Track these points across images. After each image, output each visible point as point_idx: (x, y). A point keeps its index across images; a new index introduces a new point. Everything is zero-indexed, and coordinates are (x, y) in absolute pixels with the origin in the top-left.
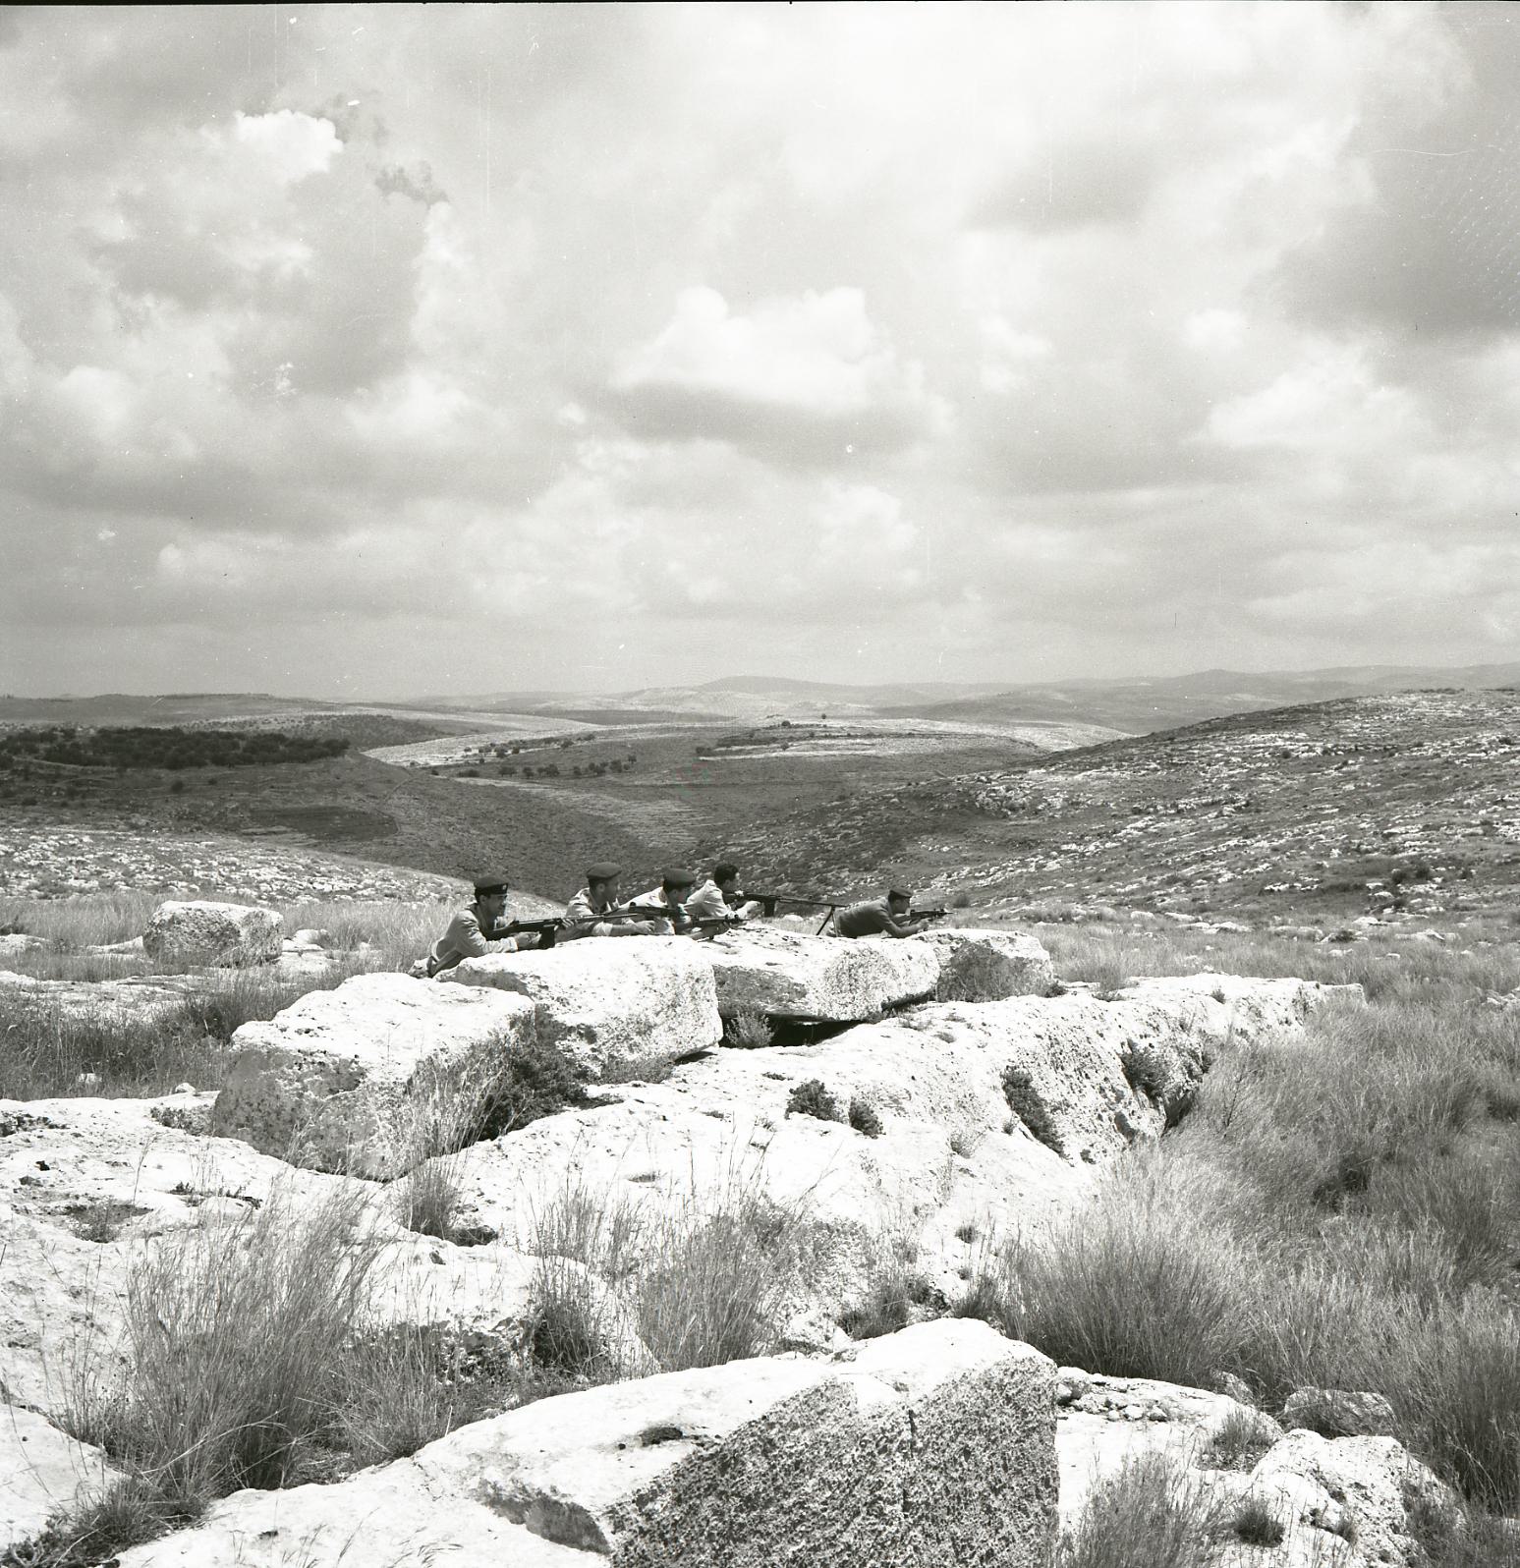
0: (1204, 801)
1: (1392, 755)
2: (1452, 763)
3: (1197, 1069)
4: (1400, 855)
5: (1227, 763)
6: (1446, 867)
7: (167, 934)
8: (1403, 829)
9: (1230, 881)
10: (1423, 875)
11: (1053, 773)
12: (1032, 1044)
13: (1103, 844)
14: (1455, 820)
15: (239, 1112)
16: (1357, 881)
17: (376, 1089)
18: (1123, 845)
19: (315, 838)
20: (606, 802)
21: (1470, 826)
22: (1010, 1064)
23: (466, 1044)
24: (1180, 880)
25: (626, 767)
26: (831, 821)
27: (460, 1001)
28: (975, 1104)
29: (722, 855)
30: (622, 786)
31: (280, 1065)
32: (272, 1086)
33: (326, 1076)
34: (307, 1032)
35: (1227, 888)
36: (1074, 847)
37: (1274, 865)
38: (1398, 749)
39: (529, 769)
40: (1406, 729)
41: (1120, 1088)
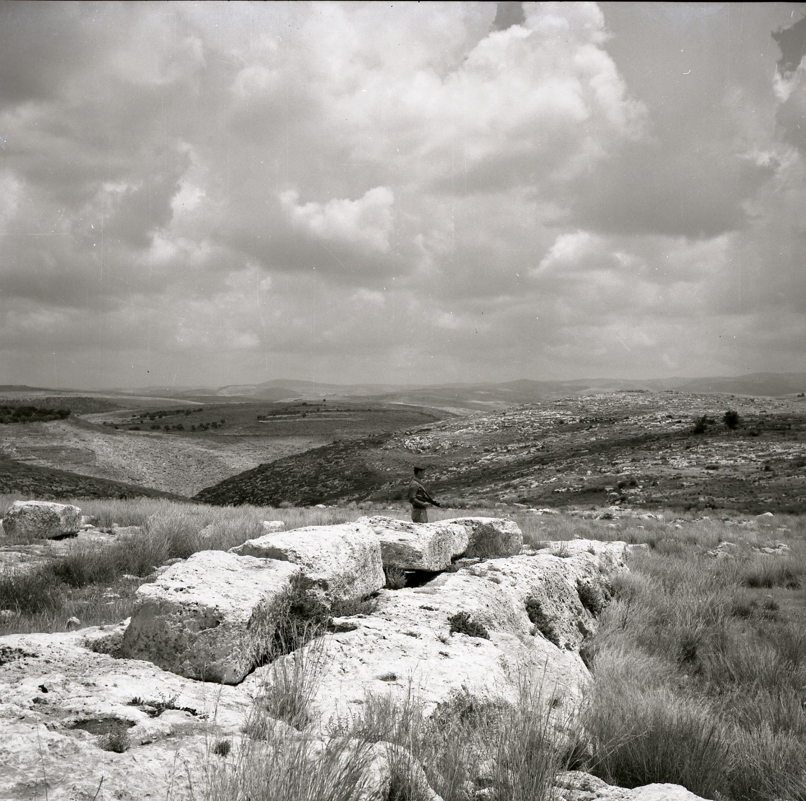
0: (521, 445)
1: (613, 423)
2: (643, 427)
3: (609, 594)
4: (621, 474)
5: (532, 426)
6: (645, 480)
7: (17, 520)
8: (622, 461)
9: (536, 487)
10: (633, 484)
11: (444, 430)
12: (537, 583)
13: (470, 467)
14: (647, 456)
15: (140, 642)
16: (601, 487)
17: (231, 626)
18: (480, 468)
19: (51, 463)
20: (209, 444)
21: (656, 460)
22: (528, 595)
23: (272, 595)
24: (511, 486)
25: (220, 426)
26: (329, 455)
27: (257, 567)
28: (516, 619)
29: (272, 473)
30: (218, 436)
31: (168, 612)
32: (163, 626)
33: (198, 619)
34: (181, 590)
35: (535, 491)
36: (455, 469)
37: (559, 479)
38: (616, 420)
39: (168, 426)
40: (620, 410)
41: (580, 608)
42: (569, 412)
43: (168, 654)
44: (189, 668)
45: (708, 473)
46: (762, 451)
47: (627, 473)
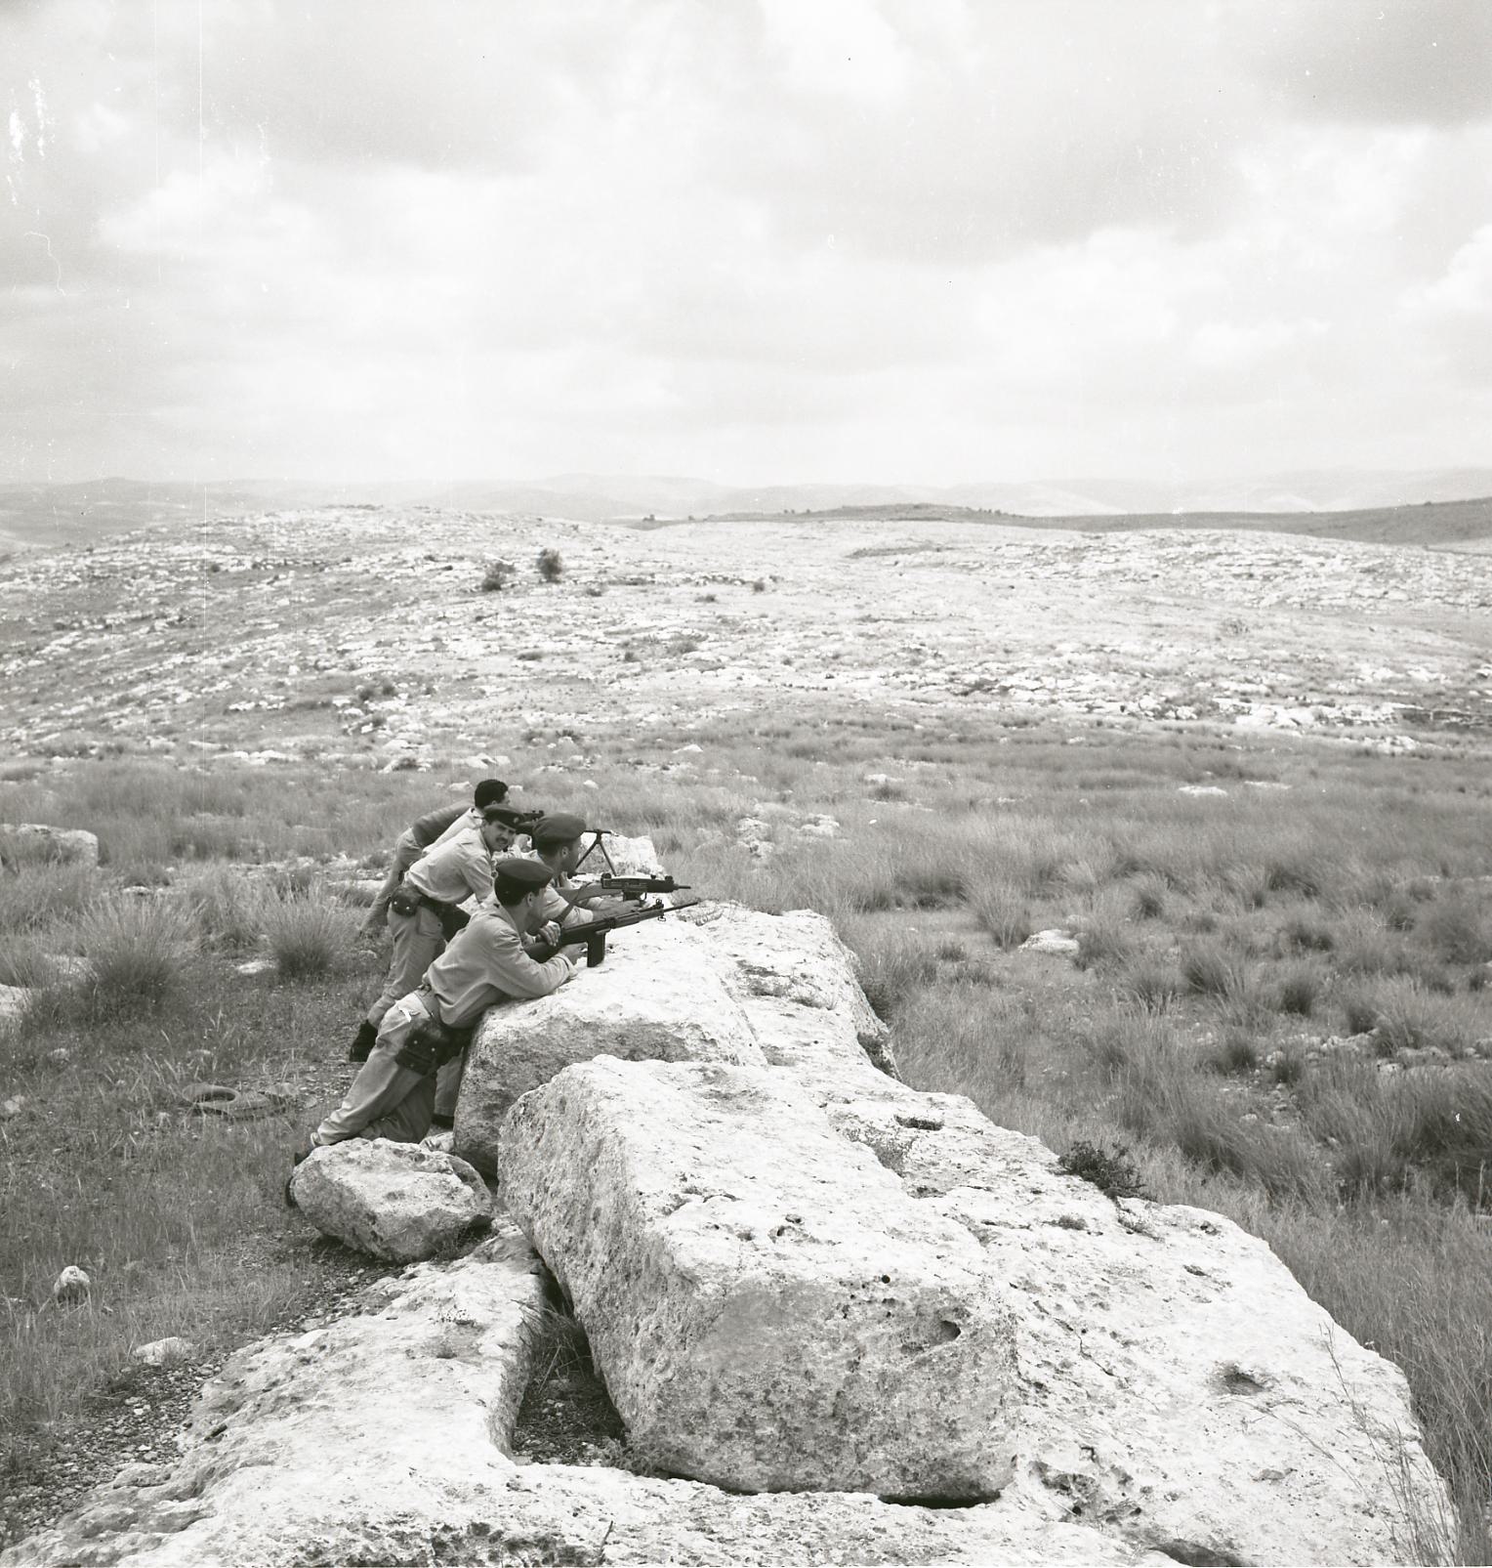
5: (153, 576)
10: (389, 692)
16: (324, 698)
32: (795, 1355)
42: (229, 549)
43: (816, 1438)
44: (884, 1470)
46: (614, 623)
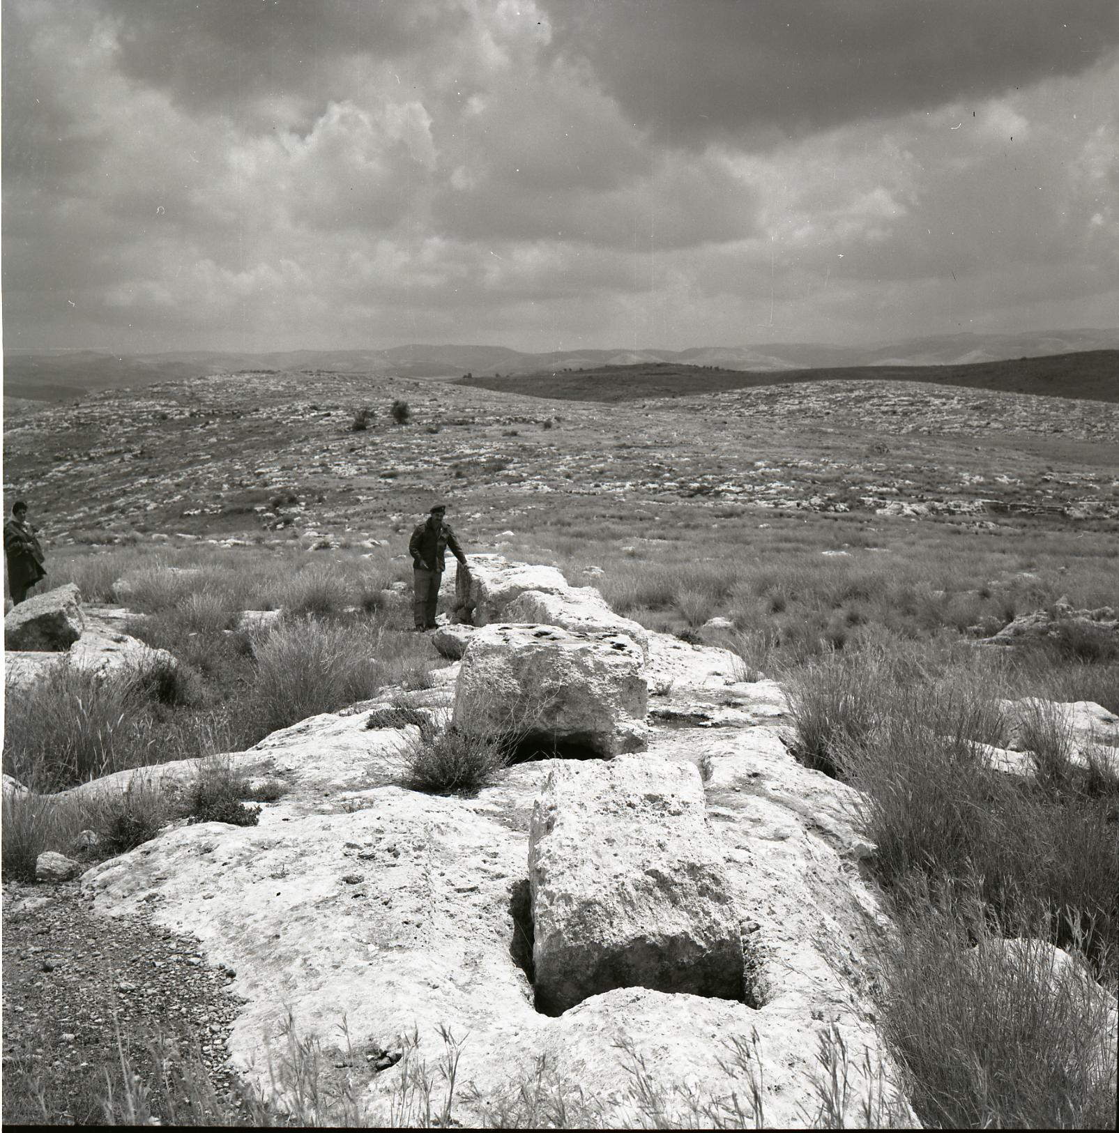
5: (121, 423)
10: (293, 501)
16: (248, 506)
42: (174, 403)
45: (386, 483)
46: (447, 452)
47: (279, 486)
